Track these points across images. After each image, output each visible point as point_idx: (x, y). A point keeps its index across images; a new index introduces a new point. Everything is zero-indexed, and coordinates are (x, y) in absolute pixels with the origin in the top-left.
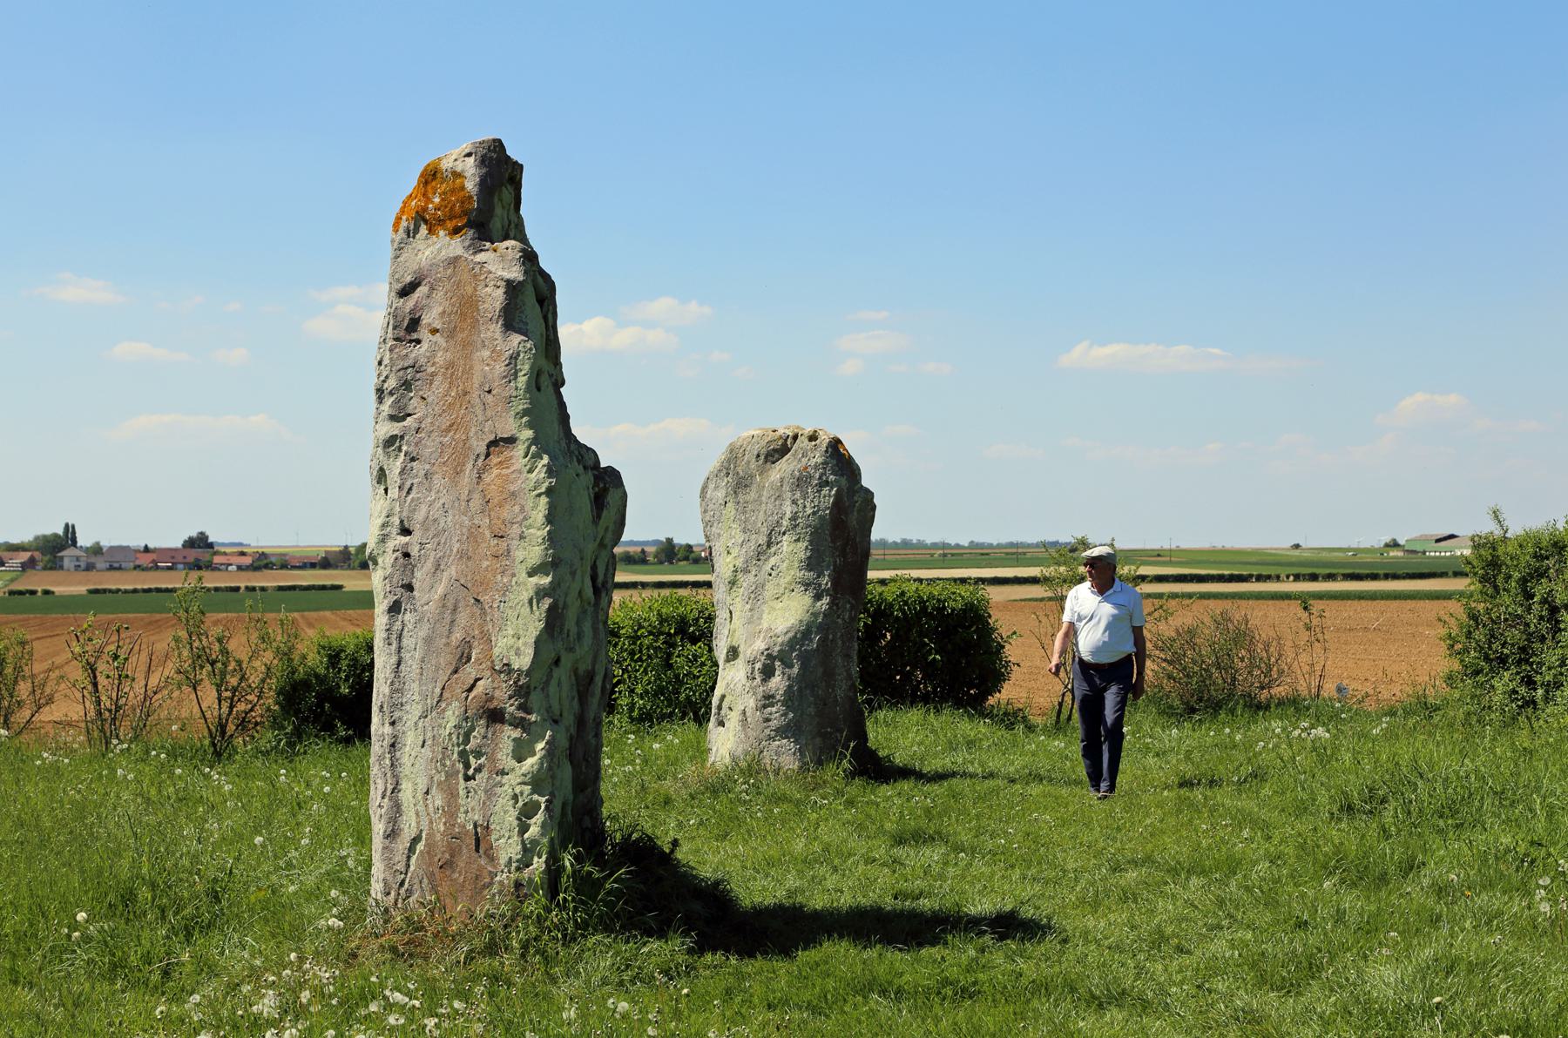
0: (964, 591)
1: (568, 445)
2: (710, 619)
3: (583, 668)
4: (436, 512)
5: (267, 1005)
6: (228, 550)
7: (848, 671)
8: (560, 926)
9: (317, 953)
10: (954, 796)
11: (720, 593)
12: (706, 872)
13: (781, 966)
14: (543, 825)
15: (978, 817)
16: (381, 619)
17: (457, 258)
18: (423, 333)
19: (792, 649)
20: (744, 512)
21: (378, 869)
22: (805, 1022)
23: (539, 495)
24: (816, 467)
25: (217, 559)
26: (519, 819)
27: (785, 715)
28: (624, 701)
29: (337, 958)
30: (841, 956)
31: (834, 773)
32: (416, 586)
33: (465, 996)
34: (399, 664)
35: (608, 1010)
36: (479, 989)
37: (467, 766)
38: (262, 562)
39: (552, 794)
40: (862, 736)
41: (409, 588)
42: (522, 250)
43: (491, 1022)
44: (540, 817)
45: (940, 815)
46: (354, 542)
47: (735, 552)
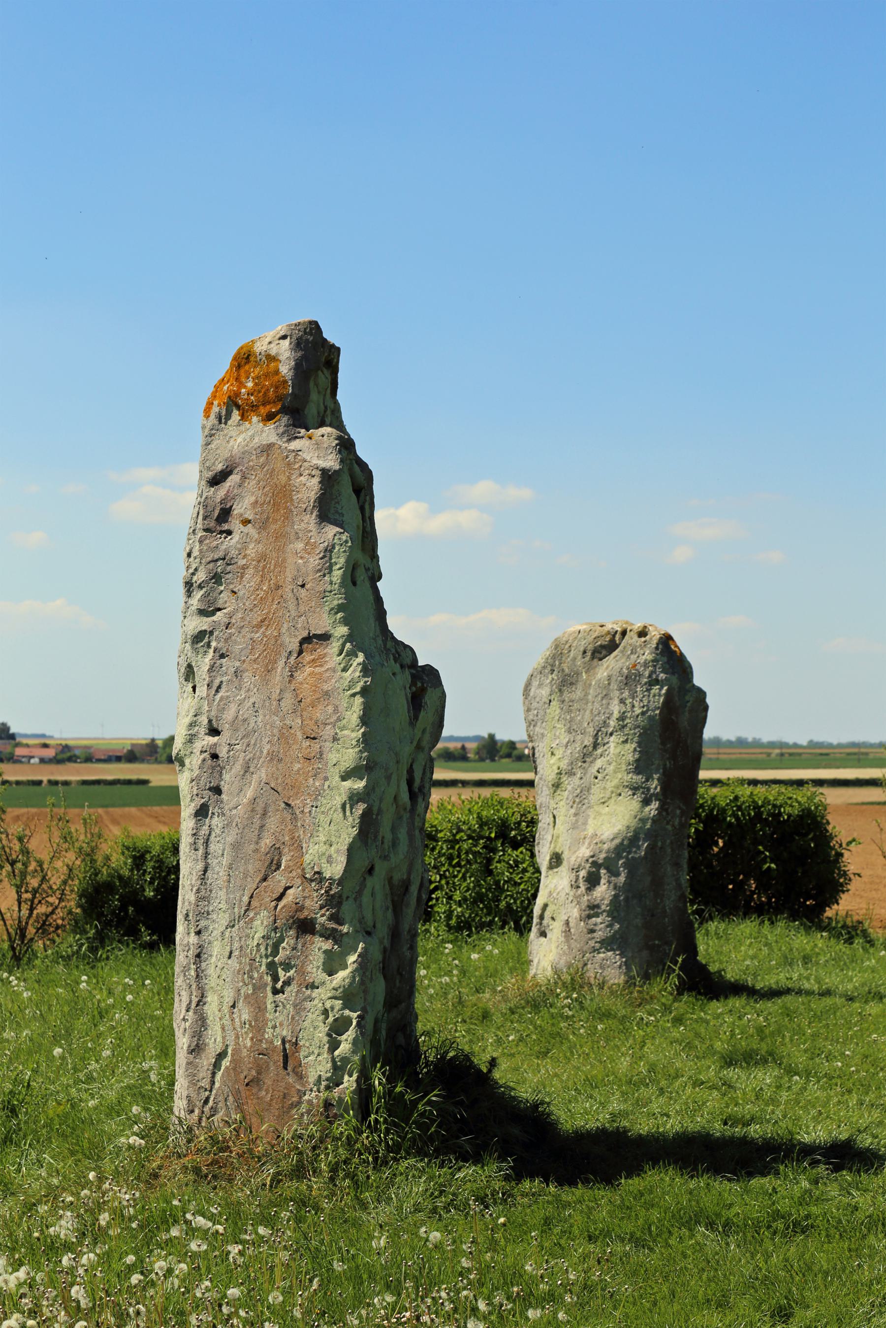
0: (801, 796)
1: (385, 642)
2: (533, 823)
3: (397, 877)
4: (244, 713)
5: (64, 1227)
6: (31, 742)
7: (677, 880)
8: (372, 1149)
9: (117, 1173)
10: (788, 1013)
11: (542, 796)
12: (525, 1093)
13: (603, 1195)
14: (355, 1042)
15: (815, 1036)
16: (187, 824)
17: (270, 446)
18: (234, 524)
19: (619, 856)
20: (569, 711)
21: (181, 1086)
22: (627, 1255)
23: (354, 695)
24: (645, 665)
25: (19, 751)
26: (329, 1035)
27: (610, 926)
28: (441, 909)
29: (138, 1178)
30: (666, 1185)
31: (662, 988)
32: (225, 788)
33: (269, 1221)
34: (205, 871)
35: (421, 1238)
36: (285, 1215)
37: (276, 979)
38: (66, 755)
39: (364, 1010)
40: (691, 949)
41: (217, 790)
42: (339, 438)
43: (297, 1251)
44: (351, 1034)
45: (772, 1034)
46: (161, 735)
47: (559, 753)
